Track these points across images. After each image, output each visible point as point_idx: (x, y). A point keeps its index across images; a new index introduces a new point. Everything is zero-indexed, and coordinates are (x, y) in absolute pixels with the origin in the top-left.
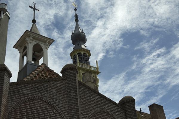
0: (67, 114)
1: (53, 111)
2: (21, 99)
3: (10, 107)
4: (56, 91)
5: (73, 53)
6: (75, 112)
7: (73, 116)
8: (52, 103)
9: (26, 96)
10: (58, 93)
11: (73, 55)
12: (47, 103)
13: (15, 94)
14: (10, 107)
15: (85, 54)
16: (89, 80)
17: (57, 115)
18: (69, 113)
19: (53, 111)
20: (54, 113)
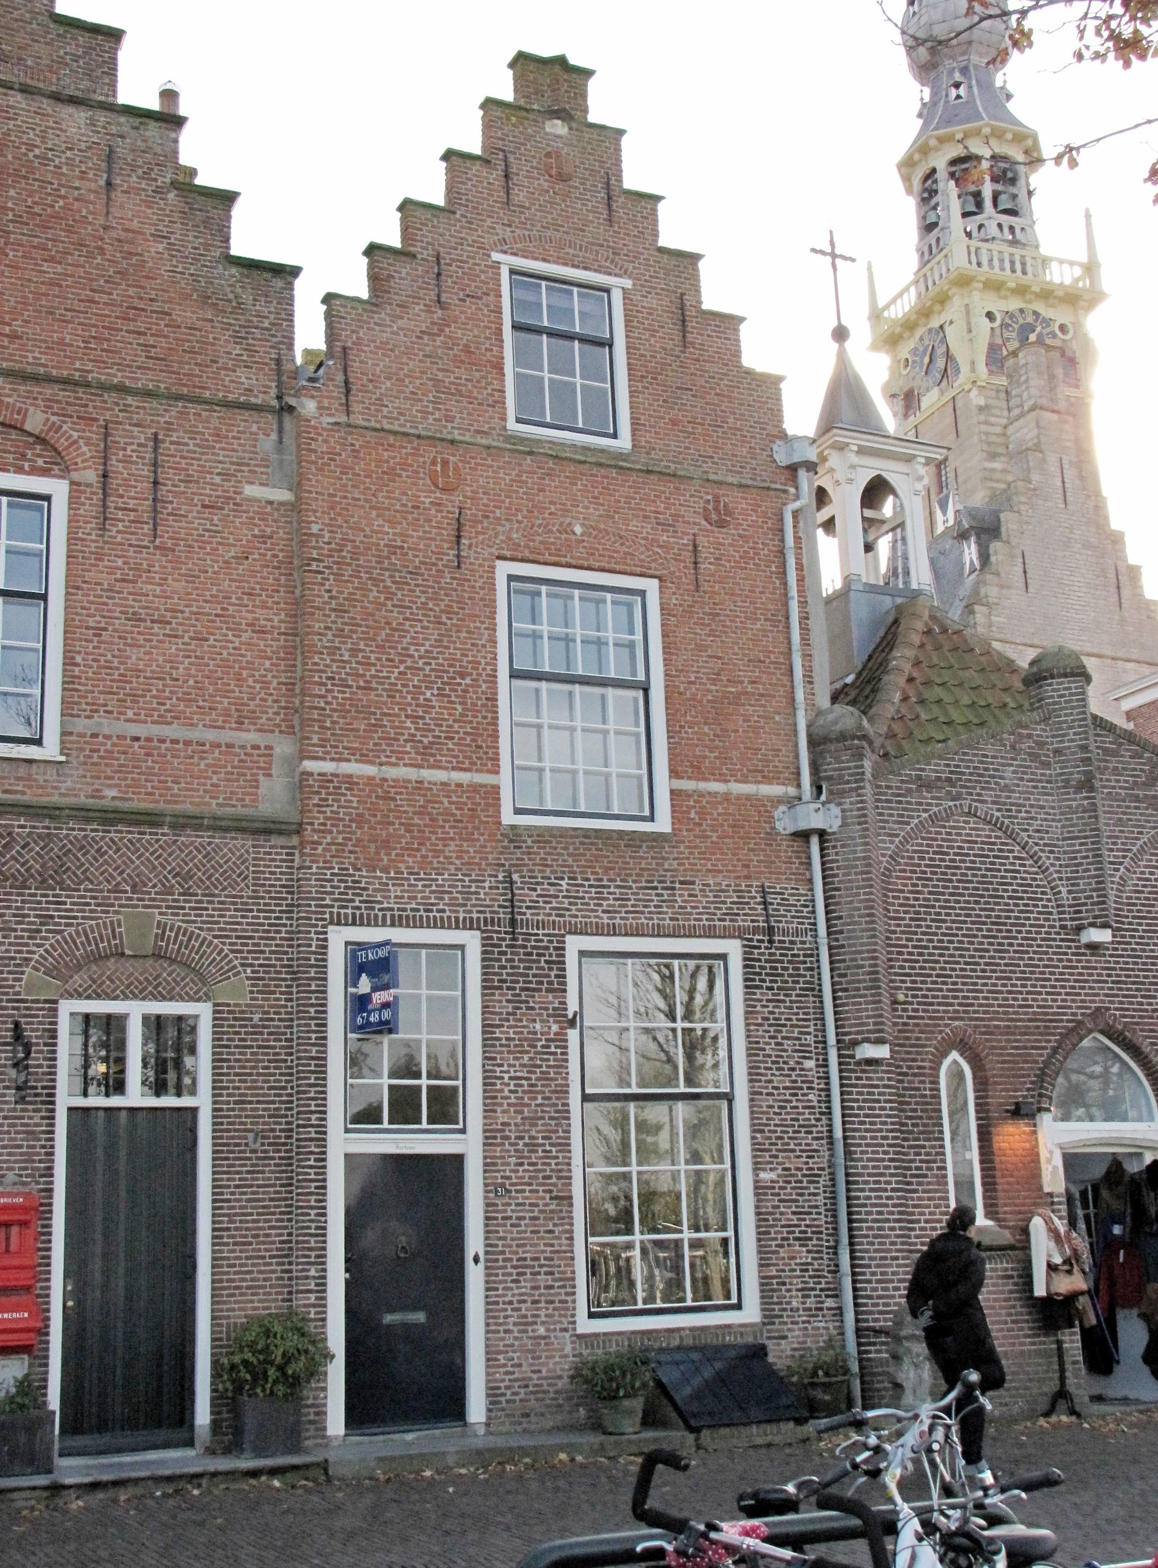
0: (1058, 859)
1: (1012, 851)
2: (908, 823)
3: (884, 855)
4: (1014, 772)
5: (917, 157)
6: (1087, 850)
7: (1081, 864)
8: (1006, 821)
9: (925, 811)
10: (1022, 779)
11: (920, 172)
12: (990, 823)
13: (891, 808)
14: (884, 855)
15: (1004, 158)
16: (1044, 401)
17: (1024, 865)
18: (1065, 852)
19: (1012, 851)
20: (1015, 858)
